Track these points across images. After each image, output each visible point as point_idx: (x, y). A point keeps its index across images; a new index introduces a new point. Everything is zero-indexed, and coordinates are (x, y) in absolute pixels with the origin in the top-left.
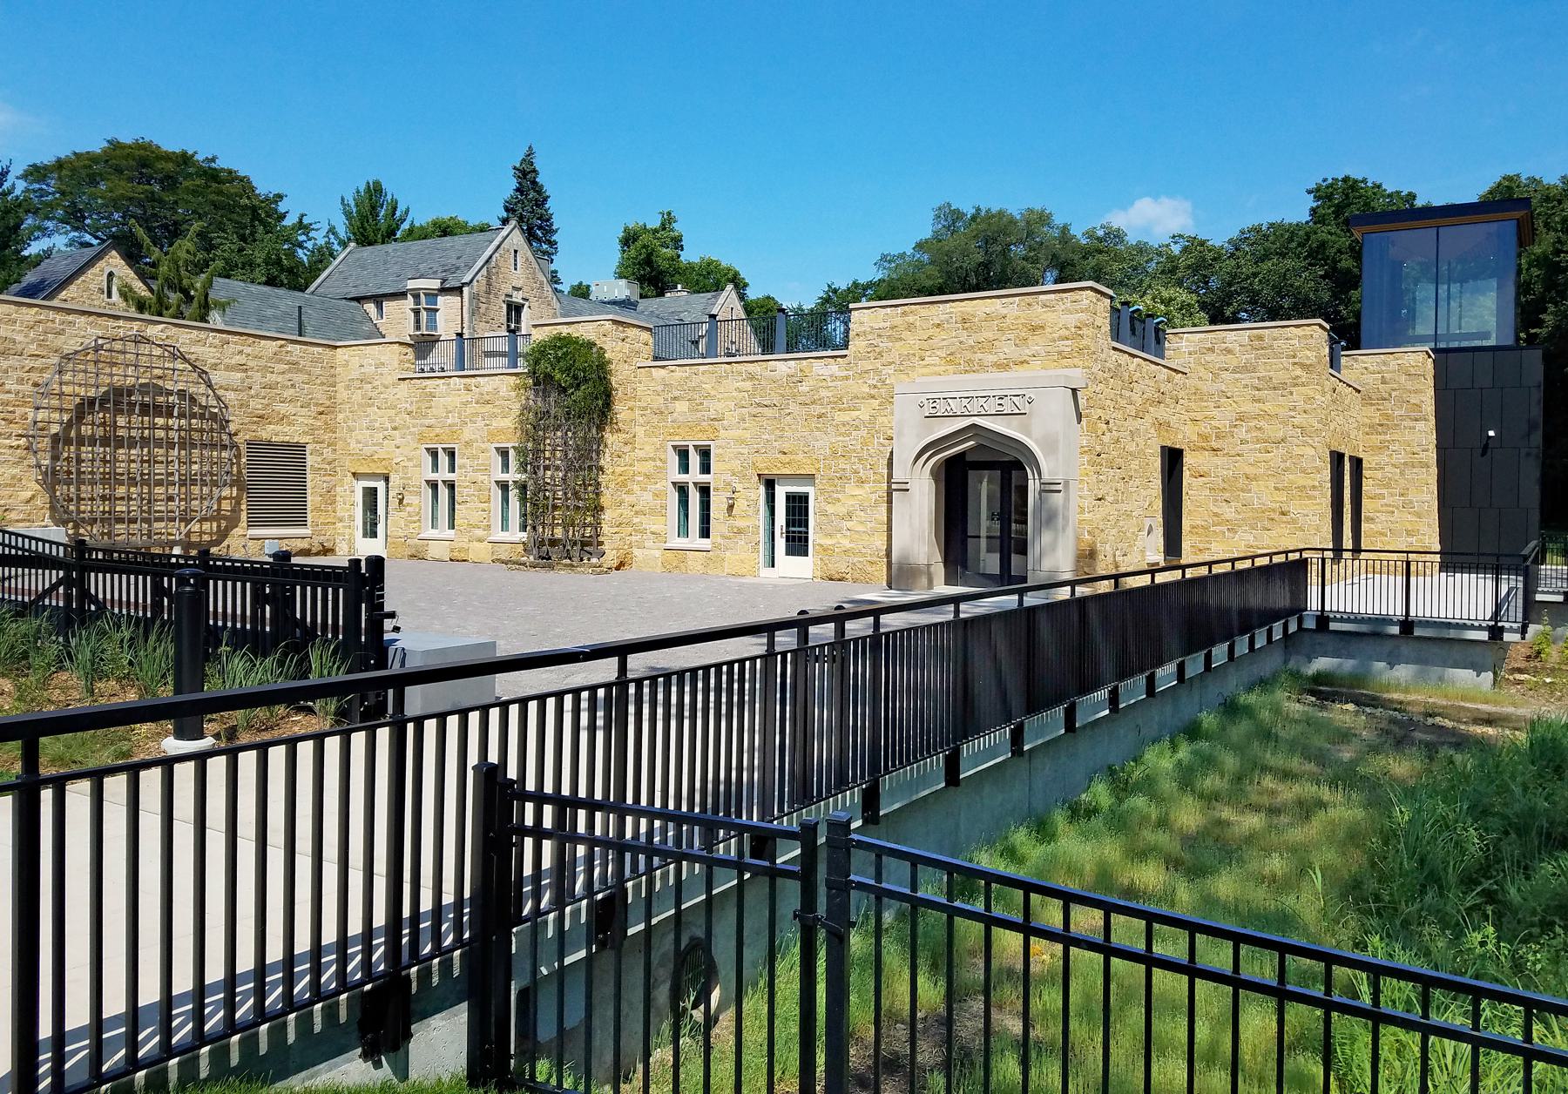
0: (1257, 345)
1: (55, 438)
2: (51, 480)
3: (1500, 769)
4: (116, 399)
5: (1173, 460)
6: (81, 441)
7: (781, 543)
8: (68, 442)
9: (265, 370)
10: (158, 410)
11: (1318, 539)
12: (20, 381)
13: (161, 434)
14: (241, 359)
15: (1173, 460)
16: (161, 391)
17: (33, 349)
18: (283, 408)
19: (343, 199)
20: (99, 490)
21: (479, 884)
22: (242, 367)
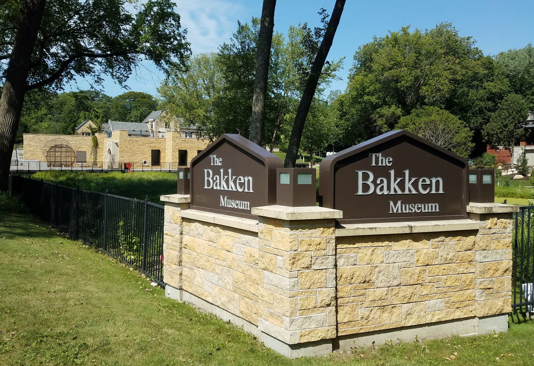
0: (200, 225)
1: (48, 152)
2: (47, 156)
3: (447, 117)
4: (56, 146)
5: (262, 331)
6: (51, 152)
7: (22, 149)
8: (49, 152)
9: (79, 141)
10: (63, 147)
11: (165, 256)
12: (43, 145)
13: (68, 151)
14: (76, 140)
15: (262, 331)
16: (63, 145)
17: (44, 140)
18: (82, 146)
19: (64, 85)
20: (53, 158)
21: (170, 181)
22: (75, 141)
